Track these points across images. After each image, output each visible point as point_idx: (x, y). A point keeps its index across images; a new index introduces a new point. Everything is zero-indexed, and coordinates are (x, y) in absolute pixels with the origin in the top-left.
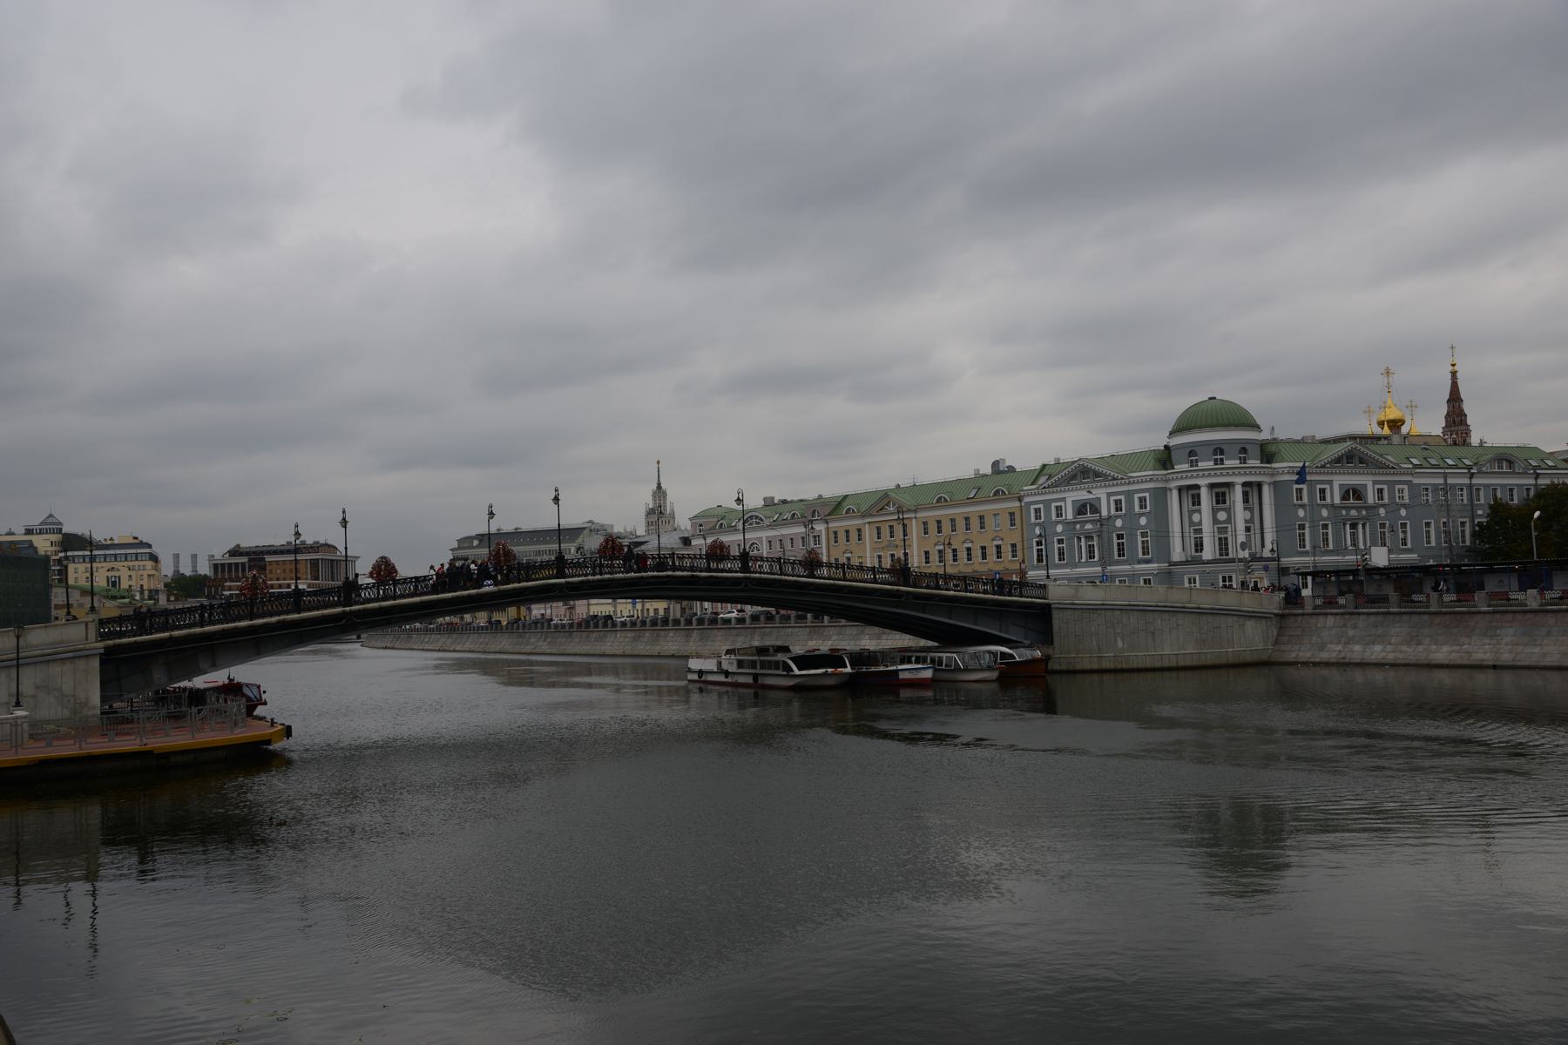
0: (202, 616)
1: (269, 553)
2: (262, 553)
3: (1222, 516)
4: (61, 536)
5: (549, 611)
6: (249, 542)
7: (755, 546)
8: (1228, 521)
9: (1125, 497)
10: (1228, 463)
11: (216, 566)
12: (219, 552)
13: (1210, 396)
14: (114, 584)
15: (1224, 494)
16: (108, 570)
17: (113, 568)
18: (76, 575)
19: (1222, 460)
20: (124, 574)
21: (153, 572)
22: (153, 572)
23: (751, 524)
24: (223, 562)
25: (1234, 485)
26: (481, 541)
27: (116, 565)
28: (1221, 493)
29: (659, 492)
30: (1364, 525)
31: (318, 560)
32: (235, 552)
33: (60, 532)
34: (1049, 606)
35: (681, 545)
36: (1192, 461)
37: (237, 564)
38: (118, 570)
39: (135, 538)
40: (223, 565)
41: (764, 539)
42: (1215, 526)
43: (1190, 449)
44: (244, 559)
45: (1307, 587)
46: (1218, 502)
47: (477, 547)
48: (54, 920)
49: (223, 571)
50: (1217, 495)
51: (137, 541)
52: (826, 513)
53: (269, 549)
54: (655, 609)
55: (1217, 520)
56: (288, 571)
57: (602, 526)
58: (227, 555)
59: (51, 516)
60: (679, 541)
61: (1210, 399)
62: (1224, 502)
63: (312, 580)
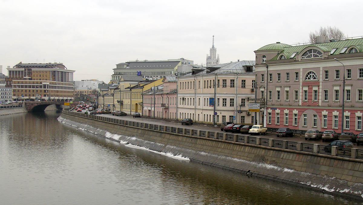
1: (33, 67)
2: (30, 66)
5: (153, 109)
6: (25, 62)
7: (312, 74)
11: (10, 72)
12: (12, 65)
23: (309, 57)
24: (13, 70)
29: (213, 50)
32: (19, 66)
35: (244, 72)
37: (19, 71)
40: (13, 71)
41: (321, 69)
44: (23, 69)
48: (18, 175)
49: (16, 75)
53: (34, 65)
54: (223, 116)
56: (36, 75)
57: (188, 61)
58: (16, 67)
60: (242, 68)
61: (277, 43)
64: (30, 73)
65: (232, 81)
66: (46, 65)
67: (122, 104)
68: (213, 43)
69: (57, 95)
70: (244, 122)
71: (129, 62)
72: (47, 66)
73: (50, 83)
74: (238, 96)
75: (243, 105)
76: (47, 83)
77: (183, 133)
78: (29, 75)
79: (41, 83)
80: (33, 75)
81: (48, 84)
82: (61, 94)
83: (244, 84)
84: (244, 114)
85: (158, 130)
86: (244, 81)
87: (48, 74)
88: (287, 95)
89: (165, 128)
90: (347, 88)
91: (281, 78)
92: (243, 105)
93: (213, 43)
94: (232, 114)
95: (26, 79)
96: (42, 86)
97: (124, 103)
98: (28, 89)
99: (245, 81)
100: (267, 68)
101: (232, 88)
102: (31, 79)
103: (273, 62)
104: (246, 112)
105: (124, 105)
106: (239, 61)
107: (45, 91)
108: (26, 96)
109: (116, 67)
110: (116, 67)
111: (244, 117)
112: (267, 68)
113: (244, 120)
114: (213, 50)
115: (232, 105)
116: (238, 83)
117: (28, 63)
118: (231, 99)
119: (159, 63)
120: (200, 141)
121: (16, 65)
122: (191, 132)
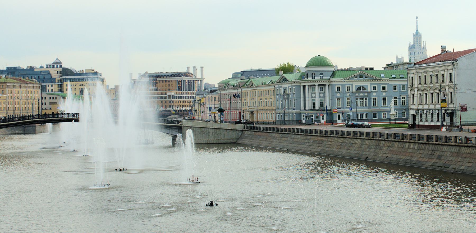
0: (28, 118)
3: (322, 95)
4: (61, 68)
8: (324, 97)
10: (324, 78)
13: (319, 55)
15: (323, 88)
16: (80, 85)
17: (82, 84)
19: (322, 76)
25: (326, 85)
27: (74, 83)
28: (322, 87)
29: (417, 36)
30: (366, 99)
31: (181, 80)
34: (182, 126)
36: (313, 77)
42: (320, 99)
43: (312, 73)
45: (340, 119)
46: (321, 91)
50: (321, 88)
52: (242, 86)
55: (323, 97)
61: (318, 56)
62: (323, 91)
66: (172, 73)
68: (417, 26)
69: (184, 106)
71: (243, 71)
72: (174, 75)
73: (176, 94)
76: (173, 93)
77: (425, 140)
79: (166, 94)
81: (173, 94)
85: (333, 135)
89: (417, 137)
93: (417, 26)
96: (167, 96)
98: (164, 100)
107: (170, 102)
114: (417, 36)
117: (154, 73)
119: (271, 71)
120: (389, 143)
122: (340, 133)
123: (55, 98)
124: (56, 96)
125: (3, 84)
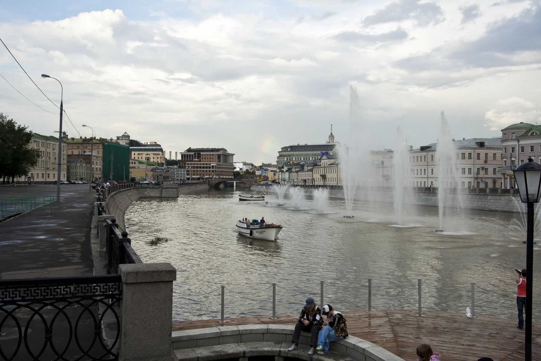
2: (199, 151)
6: (194, 147)
9: (251, 172)
11: (182, 155)
14: (148, 160)
18: (135, 156)
20: (151, 156)
21: (162, 156)
22: (162, 156)
26: (291, 149)
27: (141, 152)
32: (189, 150)
33: (129, 140)
37: (190, 155)
38: (150, 155)
39: (156, 143)
40: (185, 155)
44: (193, 153)
47: (290, 151)
51: (156, 144)
56: (204, 158)
59: (126, 133)
61: (521, 123)
63: (218, 162)
64: (199, 156)
65: (470, 154)
67: (325, 178)
68: (331, 130)
70: (479, 186)
74: (475, 166)
75: (478, 173)
78: (198, 158)
79: (210, 164)
80: (201, 158)
81: (216, 165)
82: (227, 173)
83: (479, 156)
84: (479, 180)
86: (479, 154)
87: (214, 157)
88: (505, 151)
90: (513, 159)
91: (507, 152)
92: (478, 173)
93: (331, 130)
94: (470, 180)
95: (195, 161)
97: (327, 177)
98: (199, 169)
99: (487, 154)
100: (518, 142)
101: (470, 160)
102: (200, 161)
103: (525, 136)
104: (492, 179)
105: (328, 179)
106: (464, 139)
108: (197, 175)
109: (281, 150)
110: (281, 150)
111: (479, 182)
112: (518, 142)
113: (479, 185)
115: (470, 172)
116: (474, 156)
118: (469, 169)
121: (187, 150)
123: (134, 163)
124: (135, 161)
125: (99, 145)
